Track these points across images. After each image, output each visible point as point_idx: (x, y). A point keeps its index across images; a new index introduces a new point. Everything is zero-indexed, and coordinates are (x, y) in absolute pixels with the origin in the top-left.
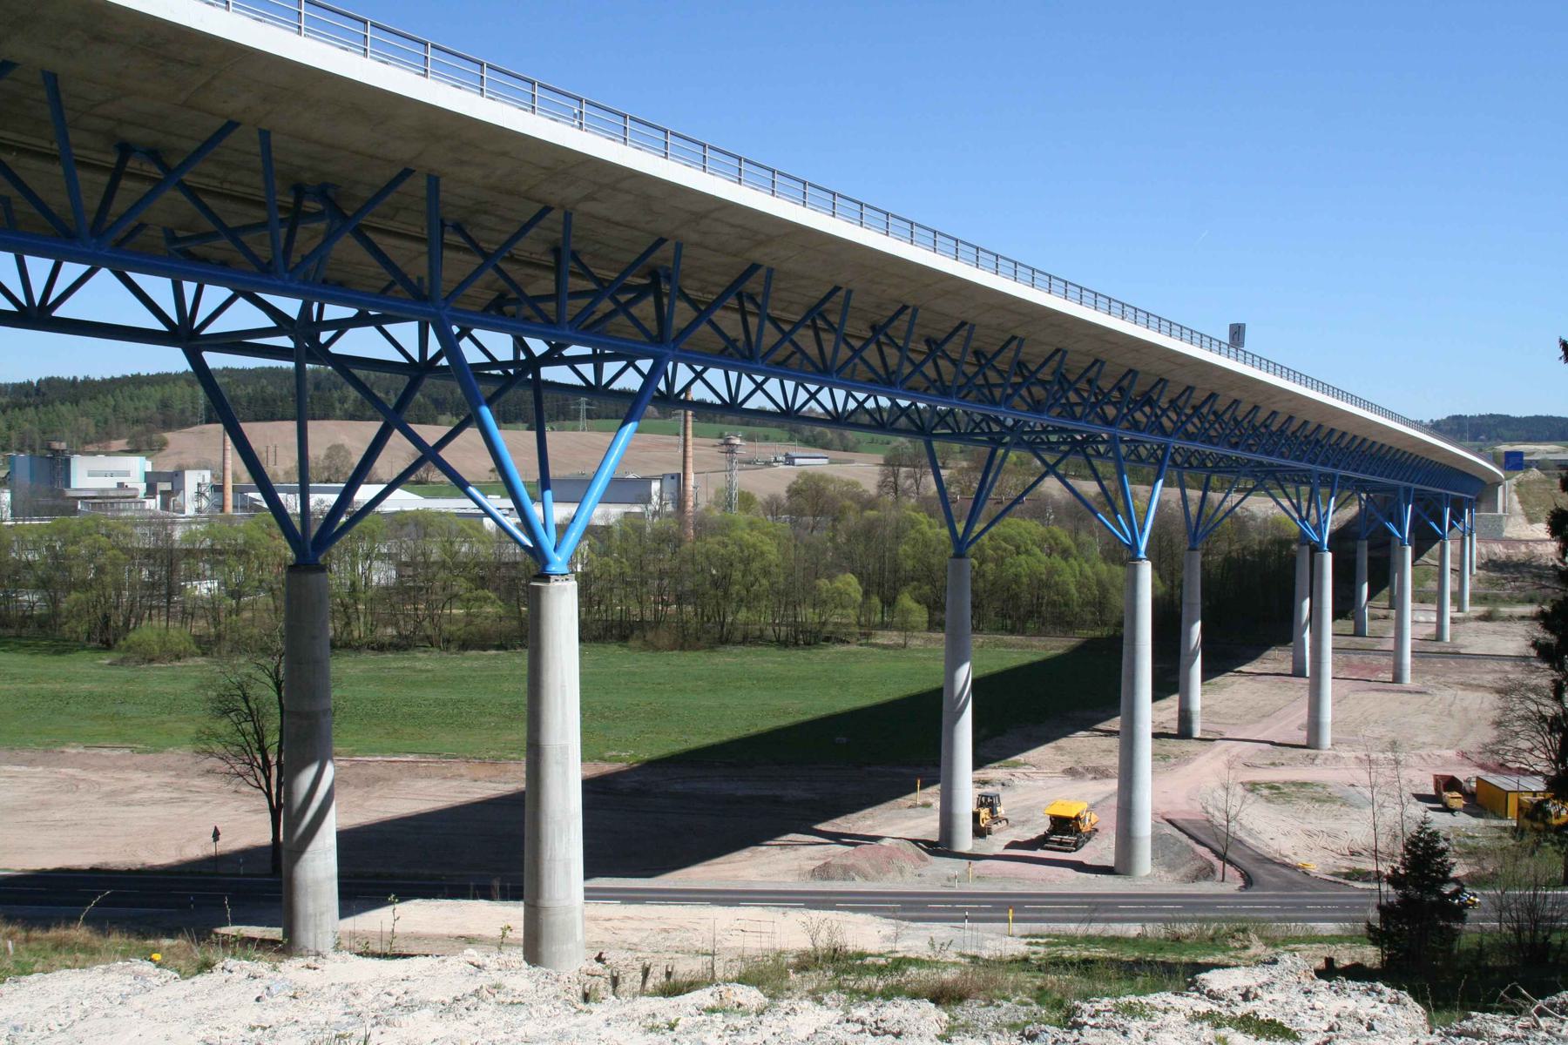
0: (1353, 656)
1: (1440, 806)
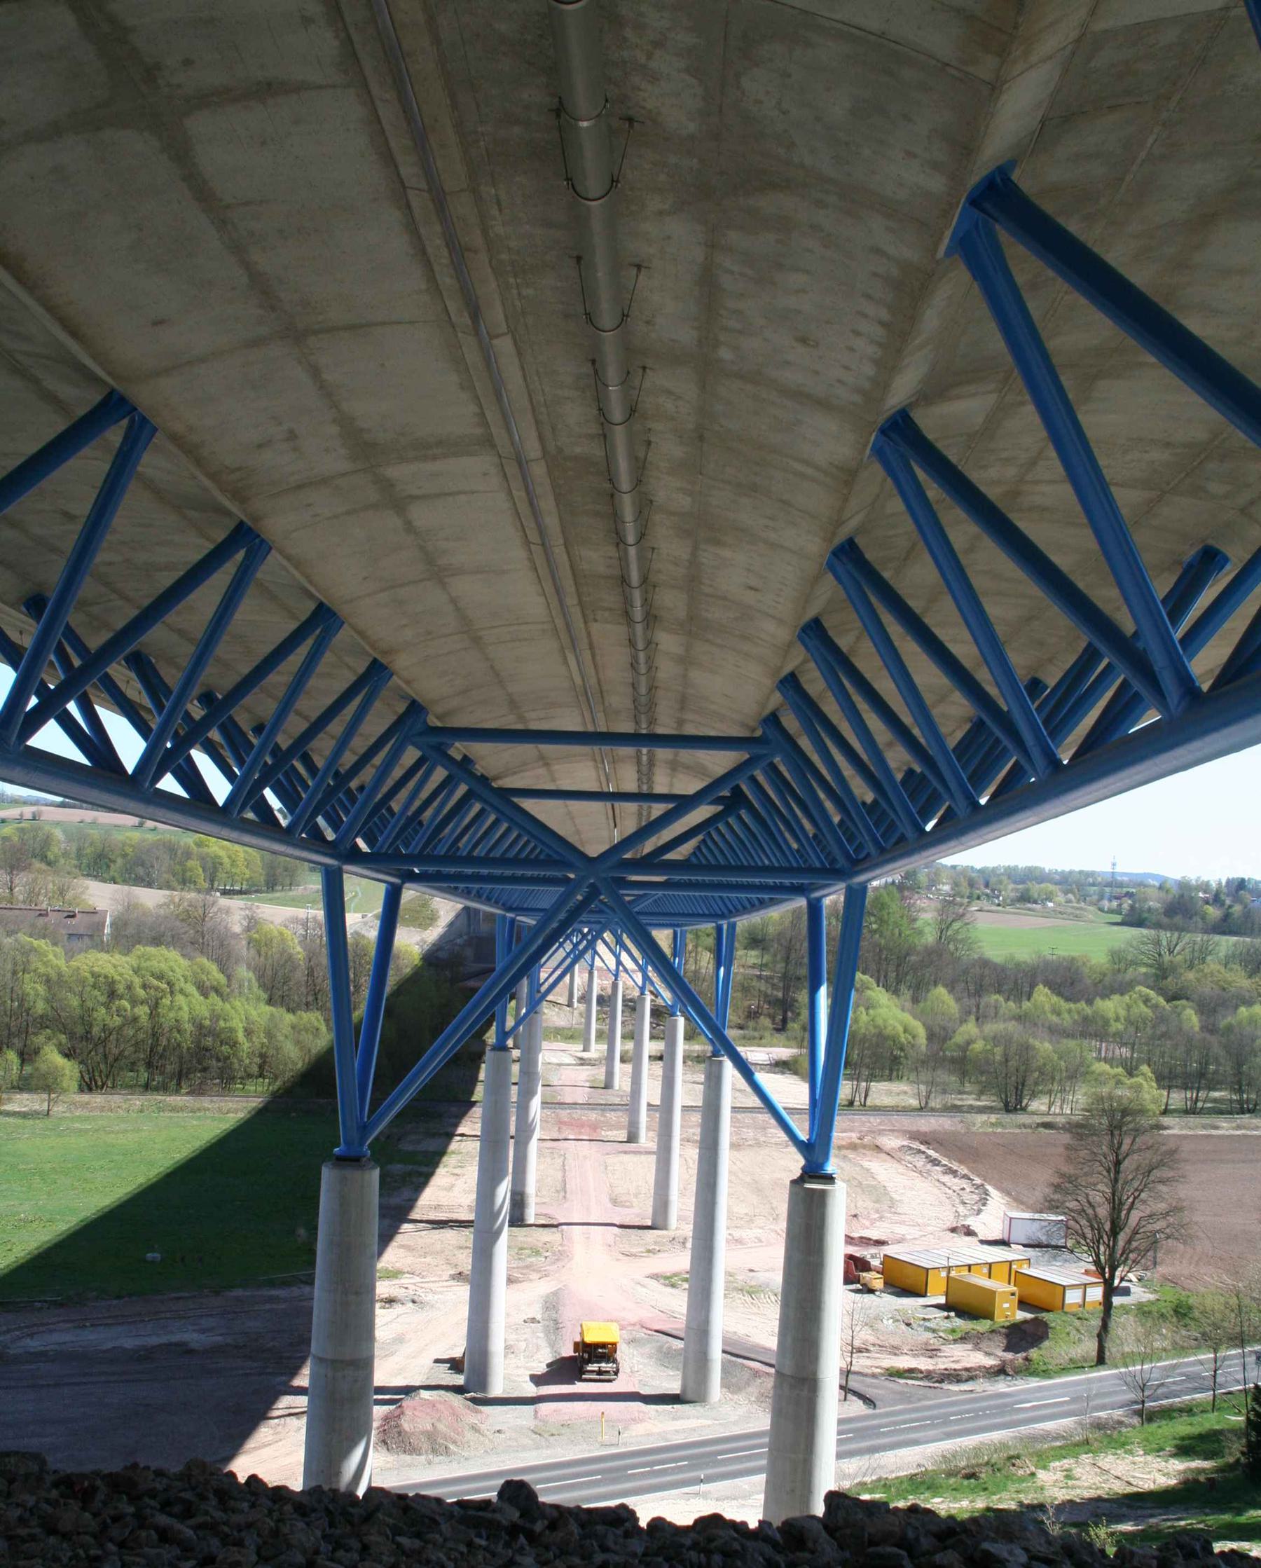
0: (561, 1111)
1: (859, 1286)
